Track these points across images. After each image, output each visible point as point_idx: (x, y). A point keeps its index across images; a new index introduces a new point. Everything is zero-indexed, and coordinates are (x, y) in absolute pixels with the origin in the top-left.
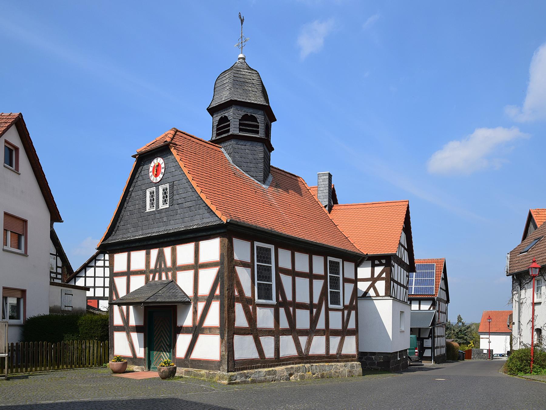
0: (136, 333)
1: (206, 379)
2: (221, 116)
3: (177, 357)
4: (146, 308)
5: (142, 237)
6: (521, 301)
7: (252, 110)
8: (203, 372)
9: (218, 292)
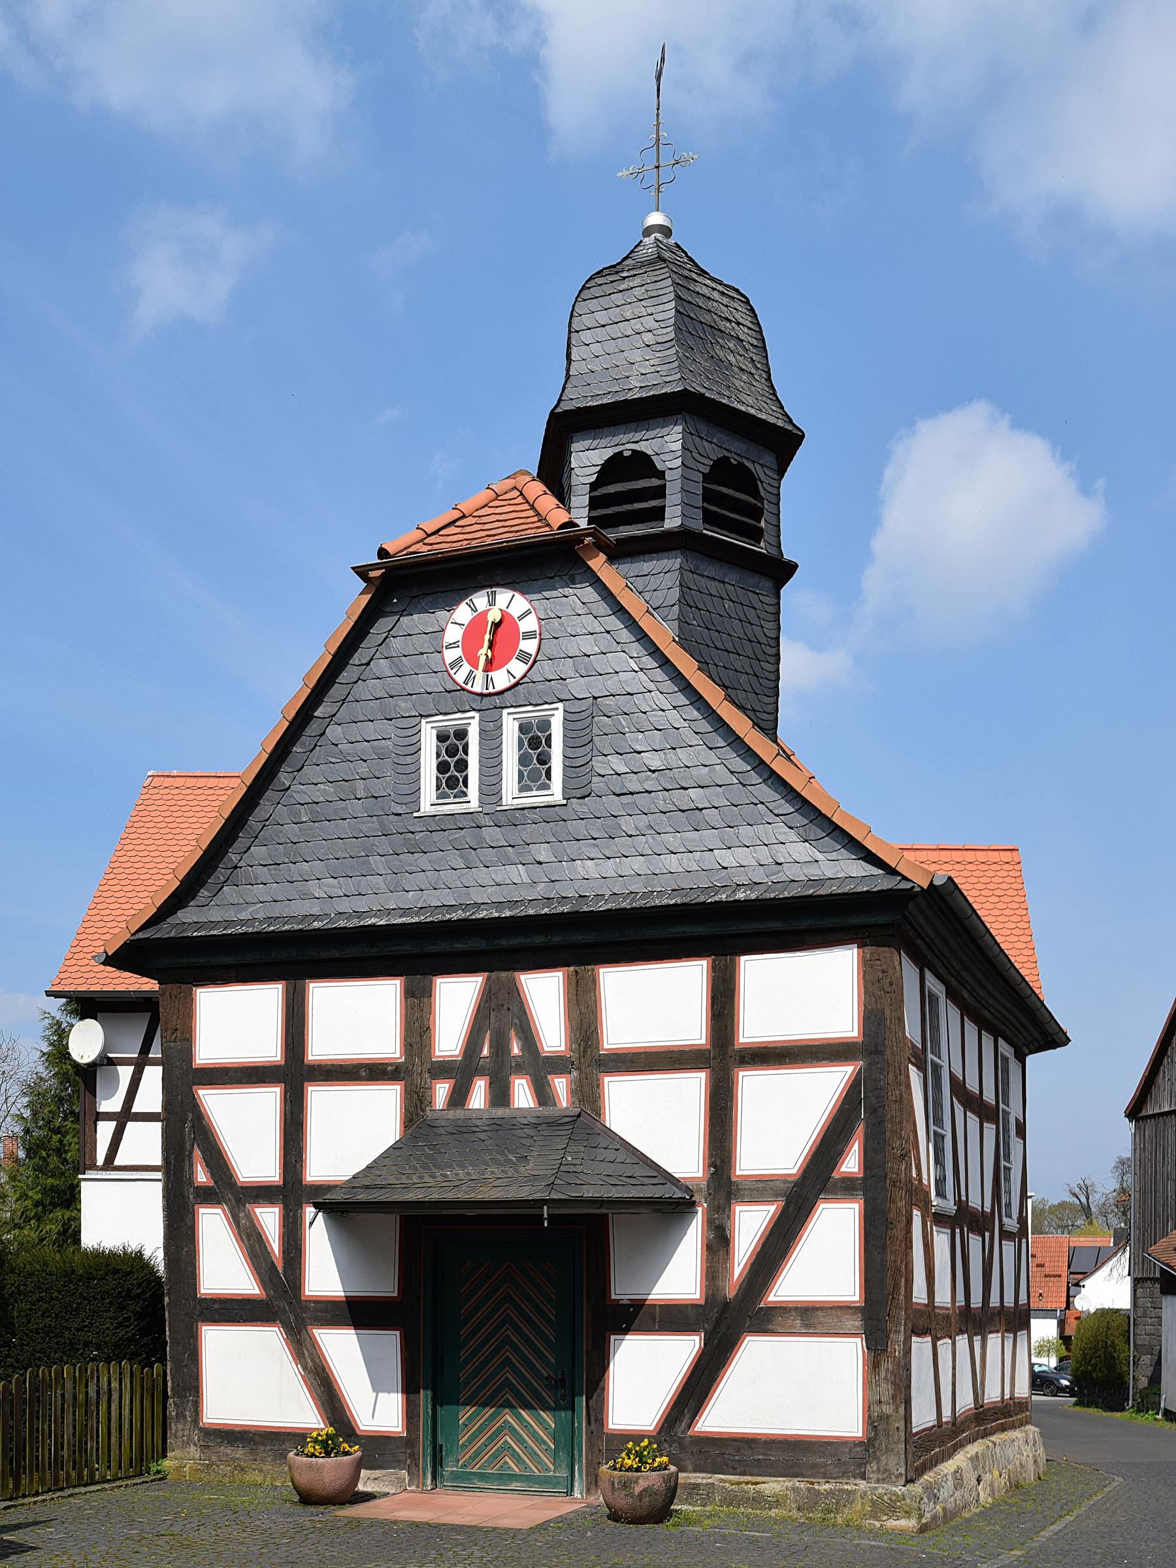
1: (795, 1513)
2: (617, 449)
5: (416, 920)
7: (741, 445)
8: (773, 1486)
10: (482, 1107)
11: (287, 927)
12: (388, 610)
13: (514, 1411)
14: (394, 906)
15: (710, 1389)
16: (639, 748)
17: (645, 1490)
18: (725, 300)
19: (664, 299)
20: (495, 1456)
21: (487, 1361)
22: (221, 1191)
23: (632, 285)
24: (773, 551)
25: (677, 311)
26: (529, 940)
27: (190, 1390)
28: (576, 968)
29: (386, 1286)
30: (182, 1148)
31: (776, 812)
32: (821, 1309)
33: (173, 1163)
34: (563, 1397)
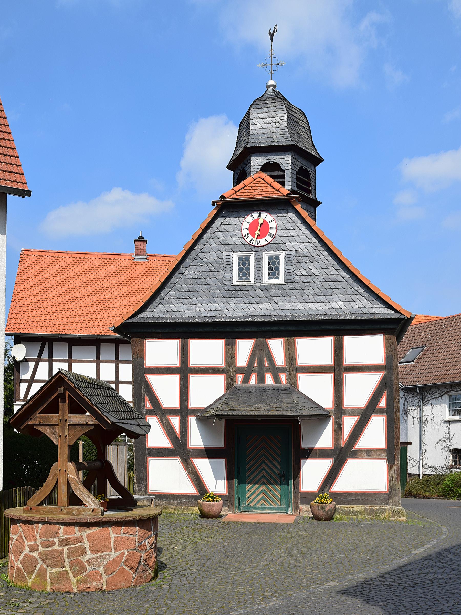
0: (208, 459)
2: (268, 161)
3: (302, 490)
4: (226, 421)
5: (234, 320)
6: (424, 418)
8: (358, 508)
9: (382, 404)
10: (255, 383)
11: (185, 321)
12: (221, 215)
13: (266, 486)
14: (225, 315)
15: (336, 477)
16: (311, 268)
17: (329, 509)
18: (299, 114)
19: (283, 112)
20: (259, 501)
21: (256, 469)
22: (156, 411)
23: (271, 106)
24: (314, 198)
25: (288, 117)
26: (272, 328)
27: (143, 481)
28: (288, 338)
29: (220, 443)
30: (141, 395)
31: (358, 291)
32: (373, 450)
33: (137, 401)
34: (284, 481)
